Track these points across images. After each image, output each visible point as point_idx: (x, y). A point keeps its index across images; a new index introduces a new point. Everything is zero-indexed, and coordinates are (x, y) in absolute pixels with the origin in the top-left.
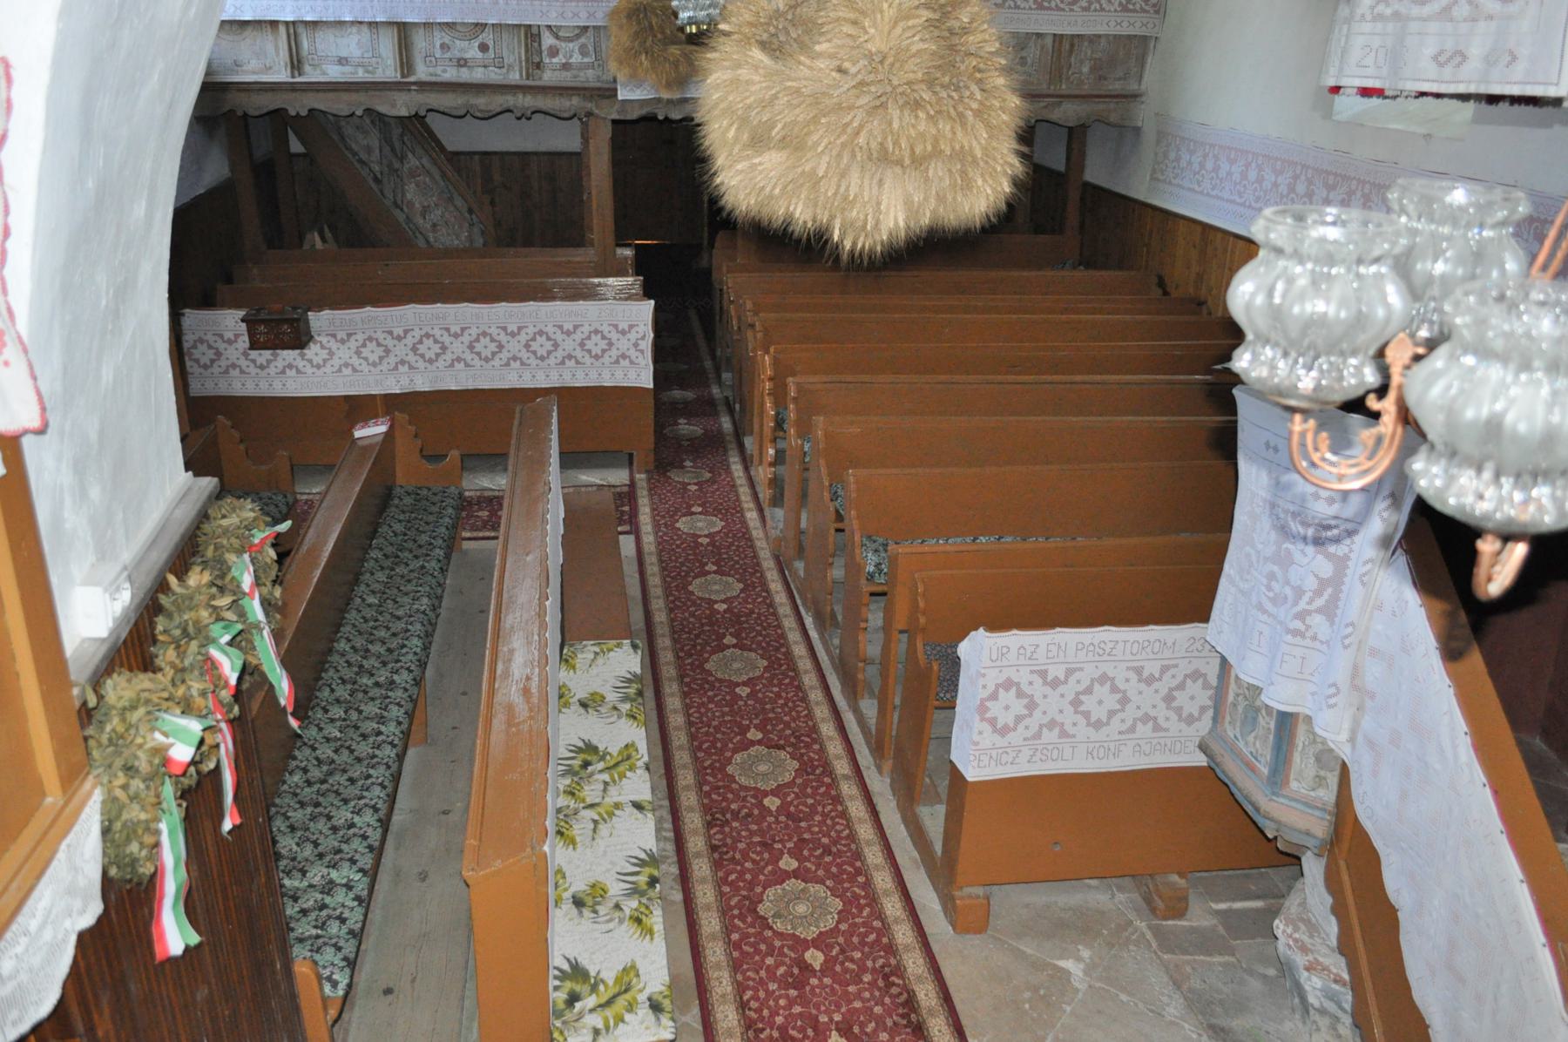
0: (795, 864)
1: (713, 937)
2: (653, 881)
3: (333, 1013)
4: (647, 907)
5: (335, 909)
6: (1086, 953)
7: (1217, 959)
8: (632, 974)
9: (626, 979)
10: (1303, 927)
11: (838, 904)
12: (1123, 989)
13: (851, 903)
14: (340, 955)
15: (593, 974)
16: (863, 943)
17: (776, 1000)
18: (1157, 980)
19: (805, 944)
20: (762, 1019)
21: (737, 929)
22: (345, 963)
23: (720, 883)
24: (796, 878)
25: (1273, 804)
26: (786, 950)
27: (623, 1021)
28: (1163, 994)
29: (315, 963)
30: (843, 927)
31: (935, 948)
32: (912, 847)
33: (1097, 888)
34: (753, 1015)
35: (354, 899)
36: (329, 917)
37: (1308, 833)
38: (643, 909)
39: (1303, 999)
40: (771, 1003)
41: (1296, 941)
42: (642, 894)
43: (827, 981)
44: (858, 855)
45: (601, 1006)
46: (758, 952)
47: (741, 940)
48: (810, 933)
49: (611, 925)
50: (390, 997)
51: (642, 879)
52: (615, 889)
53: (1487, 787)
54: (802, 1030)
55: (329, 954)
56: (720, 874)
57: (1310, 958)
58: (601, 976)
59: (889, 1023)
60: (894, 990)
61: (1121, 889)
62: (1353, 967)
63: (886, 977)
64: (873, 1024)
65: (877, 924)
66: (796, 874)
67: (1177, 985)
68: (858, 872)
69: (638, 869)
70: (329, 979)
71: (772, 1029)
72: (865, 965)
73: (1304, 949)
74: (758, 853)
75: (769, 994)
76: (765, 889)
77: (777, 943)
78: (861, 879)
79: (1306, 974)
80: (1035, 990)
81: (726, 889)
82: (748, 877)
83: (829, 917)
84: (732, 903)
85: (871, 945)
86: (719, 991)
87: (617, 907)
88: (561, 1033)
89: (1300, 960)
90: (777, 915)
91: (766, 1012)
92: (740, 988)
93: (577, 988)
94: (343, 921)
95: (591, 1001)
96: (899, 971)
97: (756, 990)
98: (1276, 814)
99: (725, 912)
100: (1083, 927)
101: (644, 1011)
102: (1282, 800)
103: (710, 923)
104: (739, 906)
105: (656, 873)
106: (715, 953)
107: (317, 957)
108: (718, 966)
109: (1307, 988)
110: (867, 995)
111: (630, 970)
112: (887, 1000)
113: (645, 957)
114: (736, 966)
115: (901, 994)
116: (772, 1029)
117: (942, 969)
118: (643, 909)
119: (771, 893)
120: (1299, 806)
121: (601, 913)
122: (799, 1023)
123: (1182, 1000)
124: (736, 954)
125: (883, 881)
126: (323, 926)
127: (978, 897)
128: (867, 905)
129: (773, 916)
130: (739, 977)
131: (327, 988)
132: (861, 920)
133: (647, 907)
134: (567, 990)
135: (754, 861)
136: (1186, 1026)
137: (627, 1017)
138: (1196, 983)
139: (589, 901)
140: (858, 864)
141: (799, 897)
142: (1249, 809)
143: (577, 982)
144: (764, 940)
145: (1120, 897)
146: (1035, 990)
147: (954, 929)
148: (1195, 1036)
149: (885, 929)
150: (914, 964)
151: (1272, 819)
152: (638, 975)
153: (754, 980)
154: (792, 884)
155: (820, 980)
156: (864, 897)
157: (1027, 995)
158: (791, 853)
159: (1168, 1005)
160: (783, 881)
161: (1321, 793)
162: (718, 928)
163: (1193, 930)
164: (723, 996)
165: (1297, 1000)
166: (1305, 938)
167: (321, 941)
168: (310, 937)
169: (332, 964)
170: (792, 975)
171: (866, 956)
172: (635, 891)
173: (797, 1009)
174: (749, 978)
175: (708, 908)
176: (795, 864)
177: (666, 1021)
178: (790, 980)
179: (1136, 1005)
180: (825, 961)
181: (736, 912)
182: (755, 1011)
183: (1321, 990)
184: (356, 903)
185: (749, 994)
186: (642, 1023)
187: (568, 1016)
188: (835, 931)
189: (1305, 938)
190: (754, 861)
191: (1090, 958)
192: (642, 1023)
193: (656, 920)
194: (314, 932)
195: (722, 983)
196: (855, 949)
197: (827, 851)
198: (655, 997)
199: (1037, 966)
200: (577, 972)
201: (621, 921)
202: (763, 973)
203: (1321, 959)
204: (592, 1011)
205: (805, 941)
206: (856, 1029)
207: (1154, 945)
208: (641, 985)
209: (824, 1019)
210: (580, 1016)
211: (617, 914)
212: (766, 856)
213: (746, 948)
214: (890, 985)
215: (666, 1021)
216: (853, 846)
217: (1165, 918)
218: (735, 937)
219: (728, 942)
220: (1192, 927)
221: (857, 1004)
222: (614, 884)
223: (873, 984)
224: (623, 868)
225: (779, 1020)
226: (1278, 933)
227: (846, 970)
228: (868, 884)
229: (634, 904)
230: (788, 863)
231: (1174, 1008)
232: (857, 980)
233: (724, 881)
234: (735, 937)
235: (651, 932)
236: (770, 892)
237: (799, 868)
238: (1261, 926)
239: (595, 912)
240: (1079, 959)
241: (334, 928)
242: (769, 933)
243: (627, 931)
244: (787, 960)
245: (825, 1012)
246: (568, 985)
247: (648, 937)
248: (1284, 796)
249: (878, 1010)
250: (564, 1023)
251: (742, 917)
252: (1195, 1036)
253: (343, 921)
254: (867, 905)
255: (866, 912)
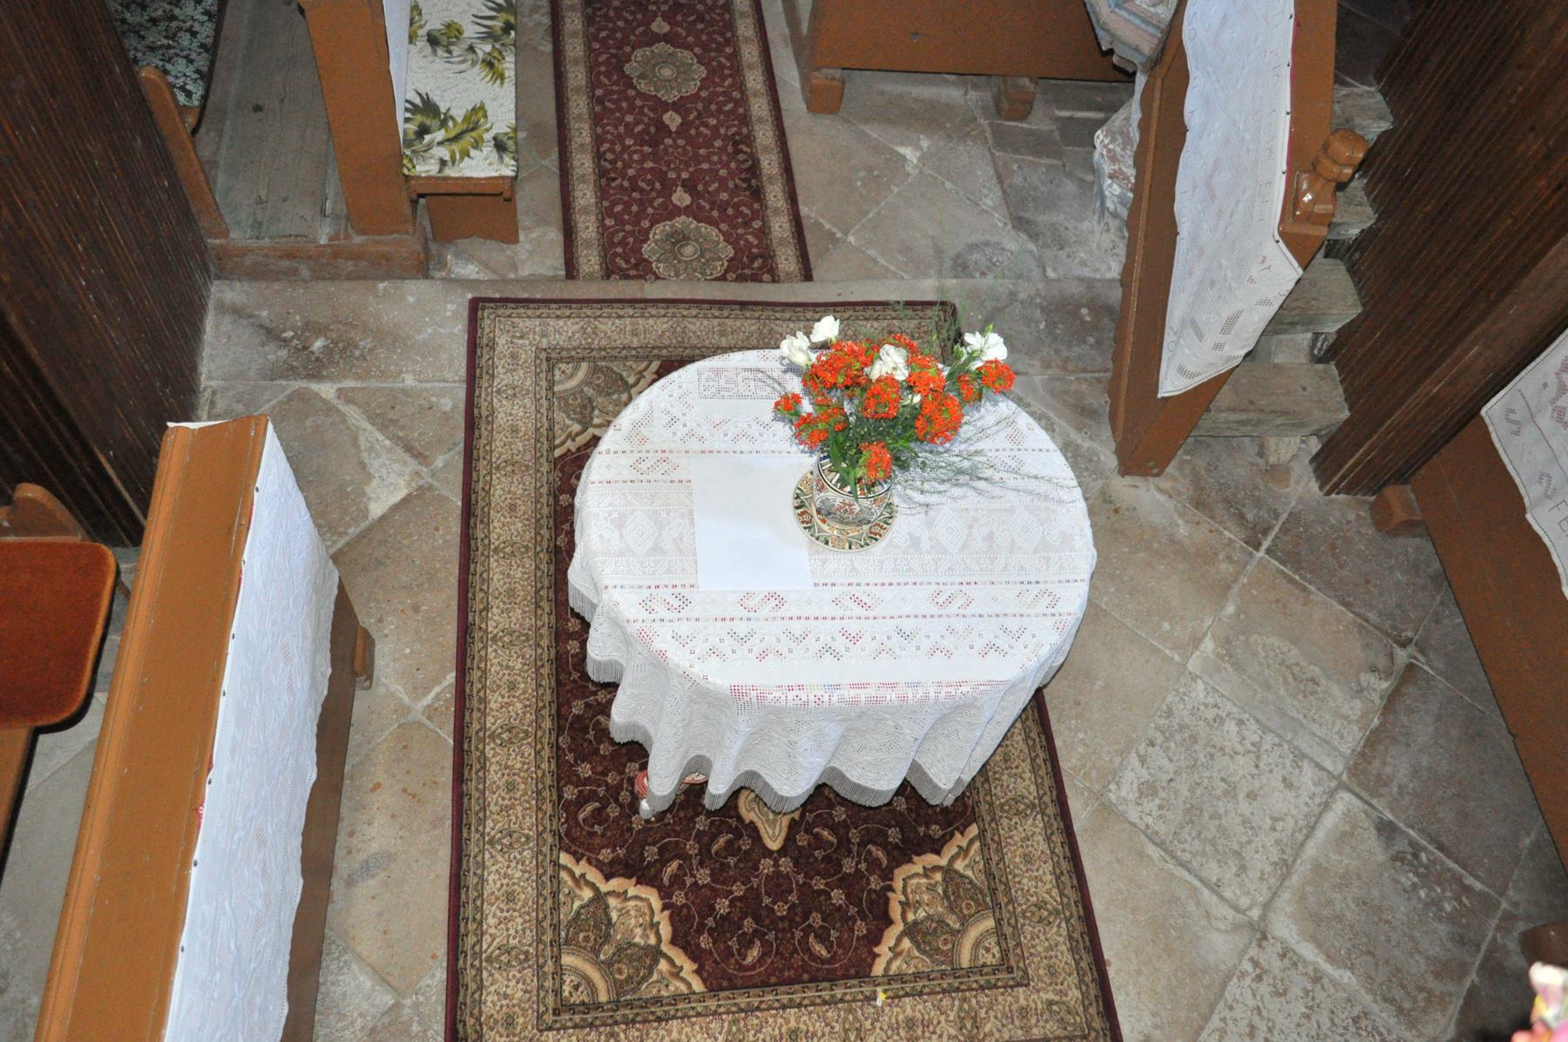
0: (666, 28)
1: (577, 90)
2: (508, 28)
3: (191, 120)
4: (500, 53)
5: (184, 22)
6: (925, 143)
7: (1044, 161)
8: (480, 113)
9: (474, 118)
10: (1120, 140)
11: (702, 72)
12: (950, 179)
13: (715, 72)
14: (192, 68)
15: (443, 110)
16: (720, 111)
17: (631, 155)
18: (983, 172)
19: (664, 106)
20: (615, 169)
21: (602, 85)
22: (197, 76)
23: (589, 39)
24: (667, 42)
25: (1112, 15)
26: (646, 110)
27: (469, 156)
28: (984, 186)
29: (166, 72)
30: (704, 94)
31: (787, 122)
32: (784, 24)
33: (953, 83)
34: (608, 165)
35: (203, 14)
36: (180, 29)
37: (1137, 49)
38: (496, 54)
39: (1103, 203)
40: (626, 156)
41: (1109, 151)
42: (496, 39)
43: (681, 142)
44: (730, 26)
45: (448, 140)
46: (619, 109)
47: (605, 95)
48: (672, 96)
49: (463, 67)
50: (260, 115)
51: (498, 24)
52: (471, 31)
53: (1292, 20)
54: (650, 183)
55: (180, 66)
56: (592, 30)
57: (1116, 167)
58: (451, 113)
59: (731, 184)
60: (741, 157)
61: (975, 86)
62: (1139, 176)
63: (736, 144)
64: (716, 185)
65: (736, 94)
66: (666, 38)
67: (1000, 179)
68: (728, 42)
69: (493, 14)
70: (183, 89)
71: (623, 179)
72: (718, 130)
73: (1113, 159)
74: (631, 13)
75: (625, 148)
76: (634, 49)
77: (638, 103)
78: (728, 50)
79: (1109, 181)
80: (870, 169)
81: (596, 46)
82: (619, 35)
83: (692, 83)
84: (600, 60)
85: (727, 114)
86: (578, 140)
87: (471, 49)
88: (411, 160)
89: (1107, 168)
90: (642, 76)
91: (620, 164)
92: (598, 140)
93: (428, 122)
94: (194, 34)
95: (440, 135)
96: (749, 140)
97: (612, 143)
98: (1112, 26)
99: (592, 68)
100: (930, 118)
101: (488, 149)
102: (1123, 13)
103: (577, 76)
104: (607, 62)
105: (512, 20)
106: (579, 106)
107: (169, 67)
108: (579, 118)
109: (1107, 193)
110: (715, 158)
111: (479, 111)
112: (733, 165)
113: (494, 99)
114: (596, 120)
115: (746, 161)
116: (623, 179)
117: (789, 144)
118: (496, 54)
119: (639, 54)
120: (1138, 22)
121: (455, 54)
122: (649, 177)
123: (1000, 194)
124: (598, 108)
125: (750, 53)
126: (173, 37)
127: (834, 79)
128: (730, 76)
129: (639, 77)
130: (599, 130)
131: (181, 98)
132: (721, 90)
133: (500, 53)
134: (417, 123)
135: (627, 21)
136: (996, 215)
137: (473, 153)
138: (1018, 180)
139: (444, 40)
140: (729, 35)
141: (667, 60)
142: (1094, 20)
143: (428, 116)
144: (627, 99)
145: (973, 94)
146: (870, 169)
147: (808, 108)
148: (1000, 224)
149: (743, 101)
150: (764, 135)
151: (1108, 31)
152: (485, 116)
153: (612, 134)
154: (661, 48)
155: (674, 140)
156: (729, 68)
157: (862, 174)
158: (665, 18)
159: (986, 196)
160: (653, 44)
161: (1160, 9)
162: (584, 82)
163: (1031, 133)
164: (582, 145)
165: (1098, 204)
166: (1118, 150)
167: (172, 51)
168: (162, 47)
169: (185, 75)
170: (648, 133)
171: (720, 123)
172: (490, 36)
173: (649, 165)
174: (608, 132)
175: (576, 61)
176: (666, 28)
177: (508, 159)
178: (647, 138)
179: (957, 192)
180: (682, 124)
181: (603, 69)
182: (610, 162)
183: (1118, 197)
184: (206, 18)
185: (606, 146)
186: (486, 159)
187: (418, 147)
188: (696, 97)
189: (1118, 150)
190: (627, 21)
191: (929, 148)
192: (486, 159)
193: (509, 65)
194: (165, 42)
195: (582, 134)
196: (712, 115)
197: (701, 18)
198: (500, 137)
199: (877, 149)
200: (427, 107)
201: (474, 64)
202: (621, 129)
203: (1125, 170)
204: (440, 144)
205: (666, 103)
206: (700, 187)
207: (991, 142)
208: (488, 126)
209: (672, 175)
210: (429, 147)
211: (470, 56)
212: (639, 16)
213: (608, 104)
214: (737, 152)
215: (508, 159)
216: (727, 16)
217: (1008, 119)
218: (599, 92)
219: (592, 97)
220: (1030, 130)
221: (705, 166)
222: (470, 26)
223: (723, 149)
224: (479, 10)
225: (631, 172)
226: (1097, 143)
227: (699, 134)
228: (735, 55)
229: (488, 48)
230: (660, 26)
231: (991, 199)
232: (708, 143)
233: (595, 37)
234: (599, 92)
235: (502, 77)
236: (639, 53)
237: (669, 32)
238: (1083, 135)
239: (450, 52)
240: (917, 147)
241: (185, 40)
242: (631, 93)
243: (477, 74)
244: (646, 120)
245: (674, 169)
246: (419, 118)
247: (498, 81)
248: (1126, 9)
249: (723, 172)
250: (413, 152)
251: (608, 75)
252: (1000, 224)
253: (194, 34)
254: (730, 76)
255: (602, 58)
